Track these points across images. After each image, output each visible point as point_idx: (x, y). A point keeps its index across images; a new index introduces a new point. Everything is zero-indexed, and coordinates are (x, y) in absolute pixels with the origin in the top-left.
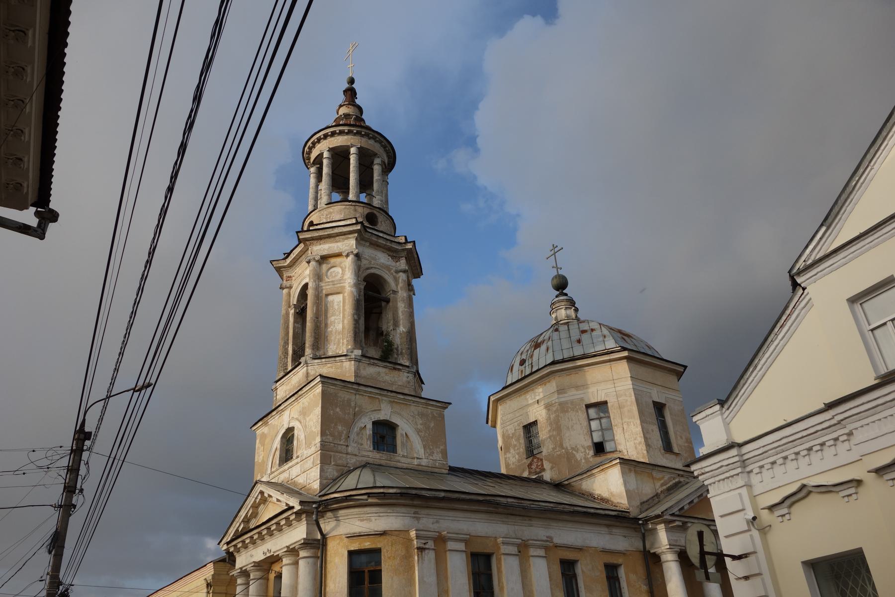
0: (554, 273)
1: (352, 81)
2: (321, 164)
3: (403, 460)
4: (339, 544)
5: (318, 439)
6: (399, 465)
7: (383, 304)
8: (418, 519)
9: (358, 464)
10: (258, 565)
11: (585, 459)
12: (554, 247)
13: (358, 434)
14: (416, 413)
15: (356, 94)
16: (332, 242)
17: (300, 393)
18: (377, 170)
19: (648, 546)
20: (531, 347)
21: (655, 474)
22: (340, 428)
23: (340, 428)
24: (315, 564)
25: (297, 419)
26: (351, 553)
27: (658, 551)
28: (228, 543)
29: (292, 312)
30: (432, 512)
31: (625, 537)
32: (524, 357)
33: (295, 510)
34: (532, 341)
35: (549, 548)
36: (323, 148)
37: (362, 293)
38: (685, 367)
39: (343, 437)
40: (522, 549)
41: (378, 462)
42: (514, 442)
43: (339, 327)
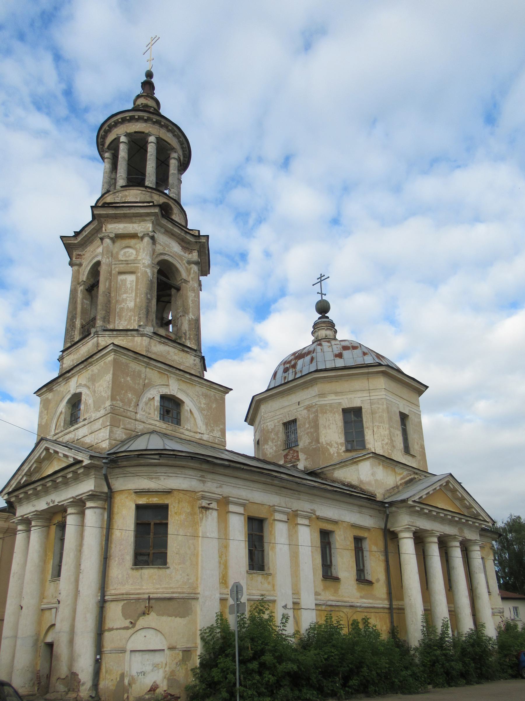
0: (319, 298)
1: (149, 75)
3: (187, 433)
5: (108, 403)
6: (183, 436)
7: (173, 291)
8: (204, 482)
9: (145, 431)
10: (40, 515)
11: (338, 453)
12: (321, 274)
13: (146, 404)
14: (200, 393)
17: (90, 360)
18: (173, 164)
22: (130, 395)
23: (130, 395)
24: (102, 515)
25: (85, 386)
26: (138, 507)
27: (397, 529)
28: (9, 493)
29: (81, 288)
31: (371, 516)
33: (84, 464)
35: (314, 518)
37: (155, 276)
38: (427, 387)
39: (133, 404)
41: (165, 431)
42: (273, 436)
43: (131, 305)
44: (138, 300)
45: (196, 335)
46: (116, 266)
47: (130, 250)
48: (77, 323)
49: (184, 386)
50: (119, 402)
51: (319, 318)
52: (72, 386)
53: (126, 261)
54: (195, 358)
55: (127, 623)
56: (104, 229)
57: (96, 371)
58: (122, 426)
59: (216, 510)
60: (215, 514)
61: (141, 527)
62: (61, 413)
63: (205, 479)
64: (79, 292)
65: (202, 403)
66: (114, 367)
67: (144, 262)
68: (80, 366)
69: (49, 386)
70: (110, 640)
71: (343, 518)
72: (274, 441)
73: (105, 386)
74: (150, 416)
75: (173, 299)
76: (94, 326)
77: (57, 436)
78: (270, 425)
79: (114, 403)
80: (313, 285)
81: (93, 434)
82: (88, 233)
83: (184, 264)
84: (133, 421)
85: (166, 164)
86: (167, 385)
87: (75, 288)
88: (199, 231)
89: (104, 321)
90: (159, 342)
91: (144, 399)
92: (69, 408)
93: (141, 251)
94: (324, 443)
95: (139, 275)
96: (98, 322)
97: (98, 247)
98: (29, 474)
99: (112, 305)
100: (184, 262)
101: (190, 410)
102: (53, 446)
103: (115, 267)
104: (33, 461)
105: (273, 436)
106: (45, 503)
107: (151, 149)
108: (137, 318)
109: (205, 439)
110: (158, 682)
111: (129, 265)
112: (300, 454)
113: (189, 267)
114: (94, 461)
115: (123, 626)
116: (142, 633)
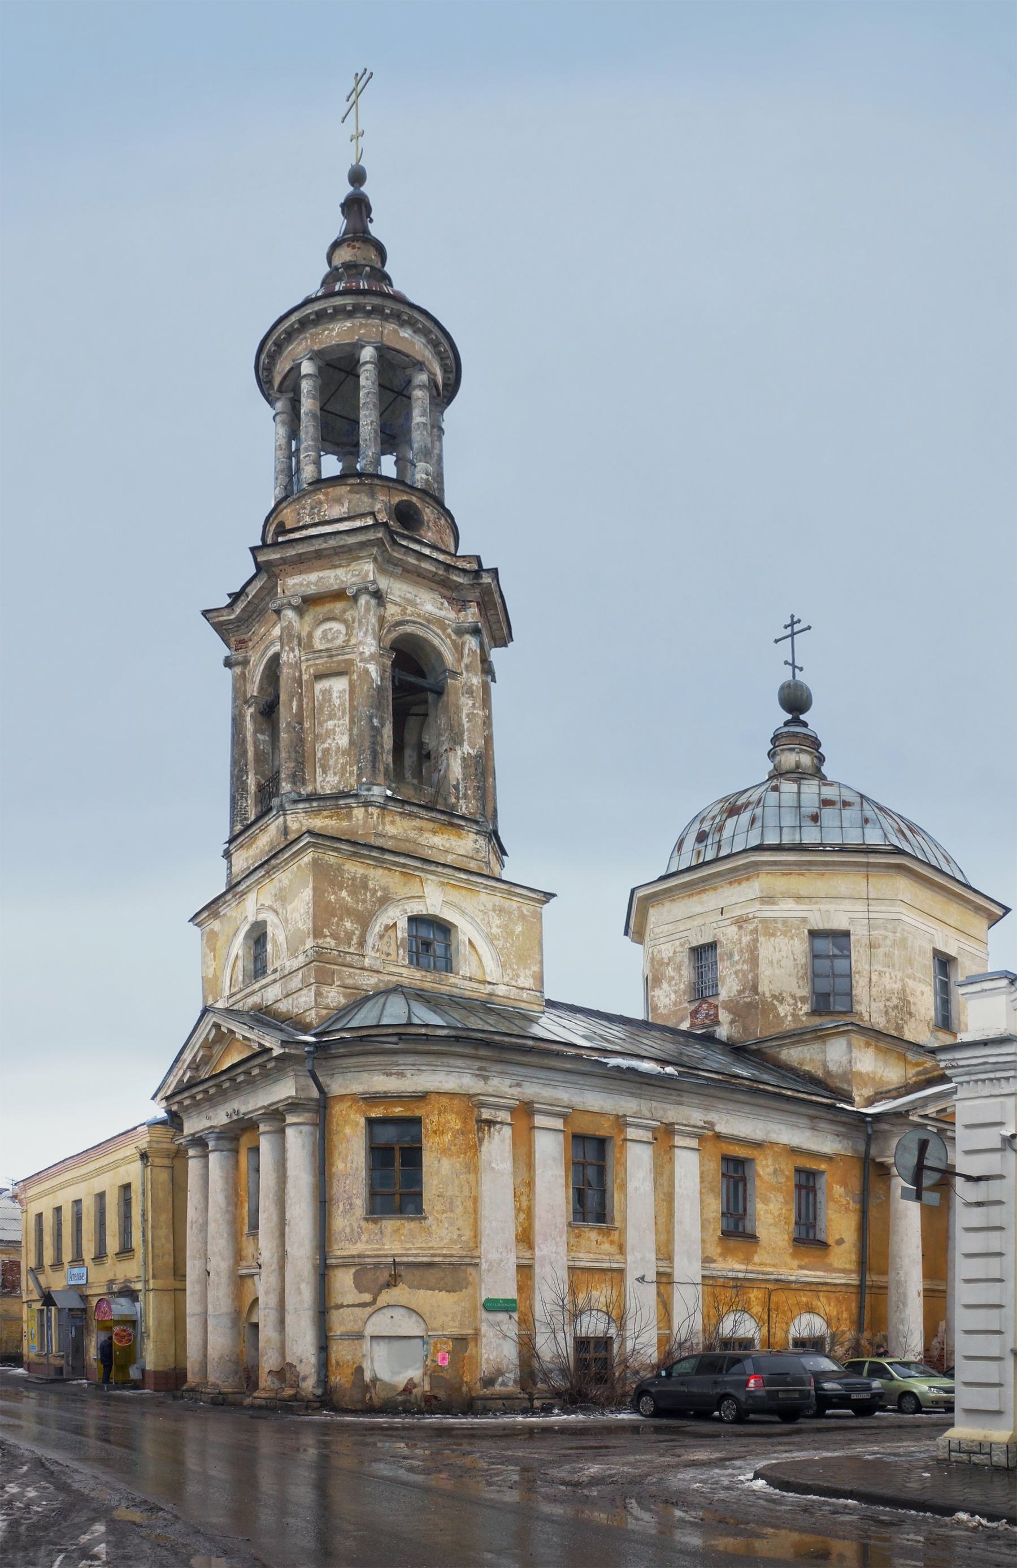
2: (296, 390)
4: (351, 1107)
7: (431, 697)
8: (486, 1079)
11: (793, 1015)
14: (490, 906)
15: (369, 210)
16: (323, 568)
17: (273, 862)
19: (873, 1151)
20: (721, 812)
21: (910, 1056)
23: (348, 925)
25: (271, 908)
26: (371, 1122)
28: (167, 1098)
30: (511, 1069)
32: (706, 827)
34: (725, 799)
35: (708, 1138)
36: (302, 359)
40: (664, 1136)
42: (670, 971)
44: (355, 731)
45: (479, 788)
46: (310, 663)
47: (335, 626)
48: (249, 781)
49: (454, 896)
50: (328, 939)
51: (787, 724)
52: (250, 908)
53: (328, 650)
54: (477, 837)
55: (367, 1297)
56: (279, 590)
57: (287, 882)
58: (338, 983)
59: (510, 1124)
60: (507, 1131)
61: (380, 1155)
62: (237, 957)
63: (488, 1074)
64: (248, 719)
65: (494, 925)
66: (314, 876)
67: (361, 649)
68: (258, 872)
69: (213, 908)
70: (341, 1322)
71: (774, 1137)
72: (673, 983)
73: (302, 911)
74: (389, 958)
75: (432, 712)
76: (277, 794)
77: (234, 999)
78: (666, 951)
79: (320, 941)
80: (776, 641)
81: (290, 999)
82: (254, 597)
83: (449, 636)
84: (358, 971)
85: (405, 396)
86: (420, 897)
87: (240, 712)
88: (478, 559)
89: (294, 783)
90: (401, 813)
91: (377, 928)
92: (250, 948)
93: (356, 625)
94: (767, 995)
95: (355, 677)
96: (284, 784)
97: (274, 625)
98: (194, 1066)
99: (308, 746)
100: (449, 631)
101: (470, 941)
102: (225, 1021)
103: (307, 667)
104: (197, 1046)
105: (670, 971)
106: (224, 1114)
107: (367, 379)
108: (355, 768)
109: (500, 994)
110: (416, 1381)
111: (335, 659)
112: (721, 1011)
113: (459, 641)
114: (290, 1049)
115: (357, 1302)
116: (388, 1312)
